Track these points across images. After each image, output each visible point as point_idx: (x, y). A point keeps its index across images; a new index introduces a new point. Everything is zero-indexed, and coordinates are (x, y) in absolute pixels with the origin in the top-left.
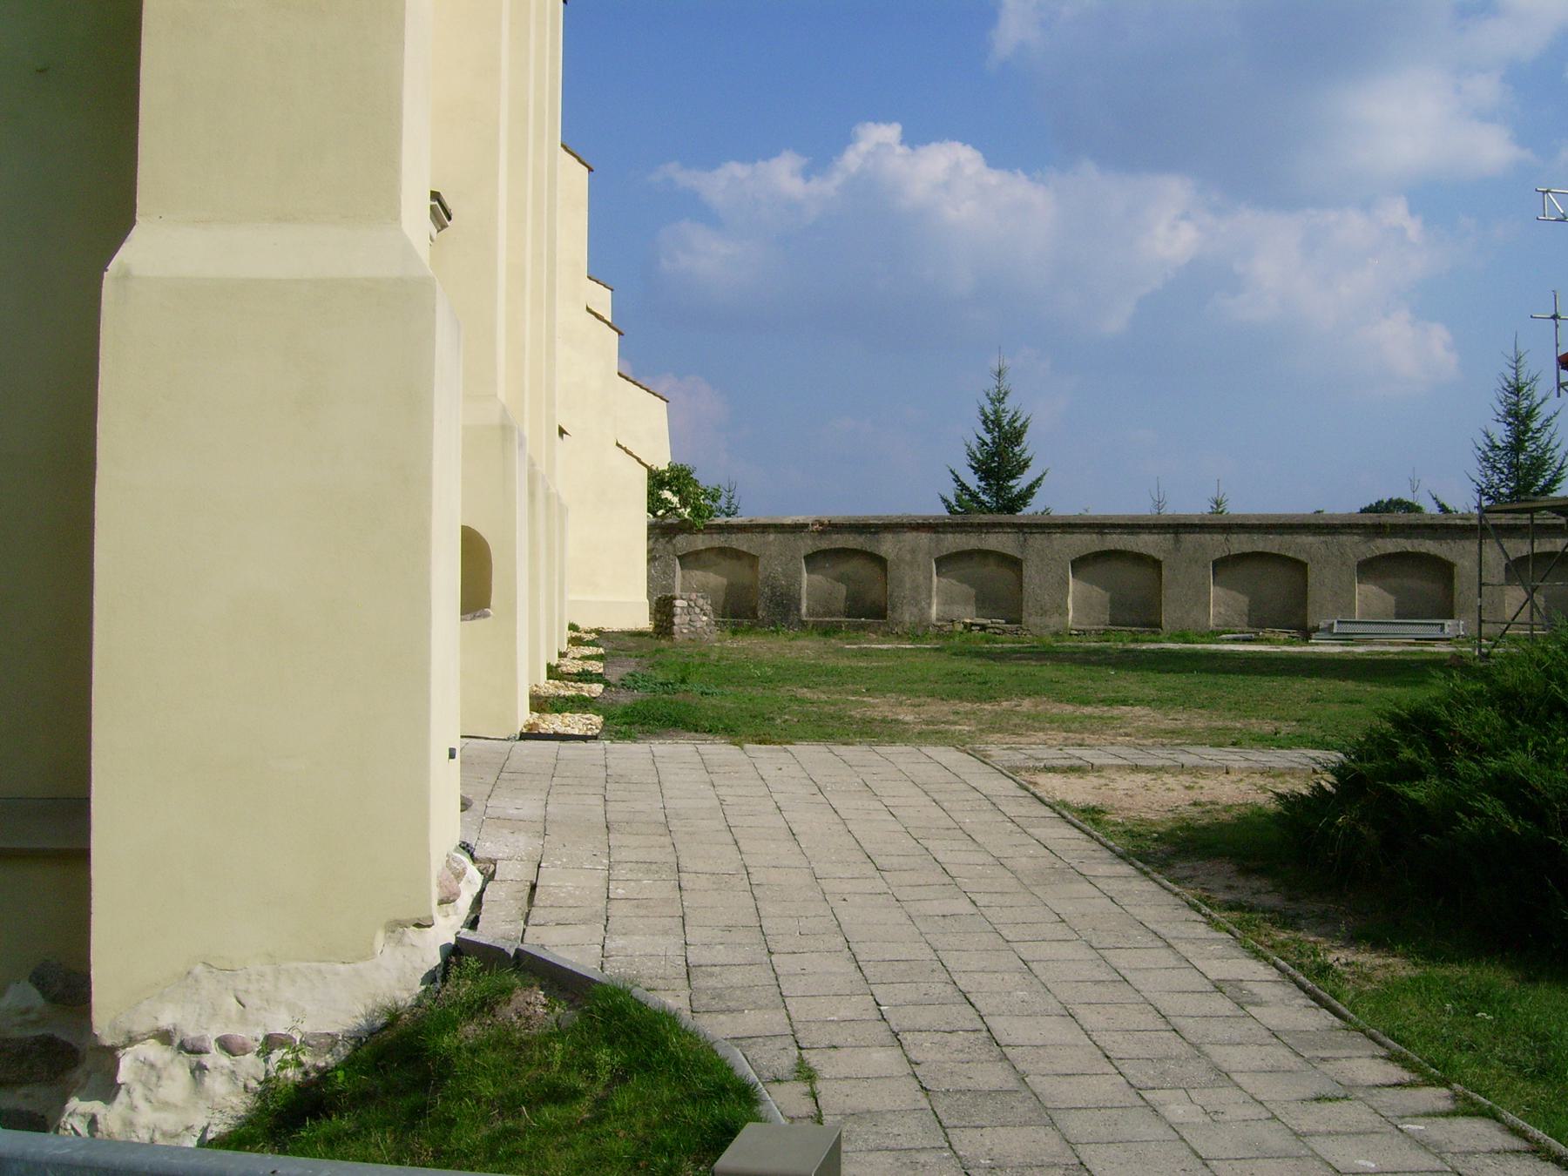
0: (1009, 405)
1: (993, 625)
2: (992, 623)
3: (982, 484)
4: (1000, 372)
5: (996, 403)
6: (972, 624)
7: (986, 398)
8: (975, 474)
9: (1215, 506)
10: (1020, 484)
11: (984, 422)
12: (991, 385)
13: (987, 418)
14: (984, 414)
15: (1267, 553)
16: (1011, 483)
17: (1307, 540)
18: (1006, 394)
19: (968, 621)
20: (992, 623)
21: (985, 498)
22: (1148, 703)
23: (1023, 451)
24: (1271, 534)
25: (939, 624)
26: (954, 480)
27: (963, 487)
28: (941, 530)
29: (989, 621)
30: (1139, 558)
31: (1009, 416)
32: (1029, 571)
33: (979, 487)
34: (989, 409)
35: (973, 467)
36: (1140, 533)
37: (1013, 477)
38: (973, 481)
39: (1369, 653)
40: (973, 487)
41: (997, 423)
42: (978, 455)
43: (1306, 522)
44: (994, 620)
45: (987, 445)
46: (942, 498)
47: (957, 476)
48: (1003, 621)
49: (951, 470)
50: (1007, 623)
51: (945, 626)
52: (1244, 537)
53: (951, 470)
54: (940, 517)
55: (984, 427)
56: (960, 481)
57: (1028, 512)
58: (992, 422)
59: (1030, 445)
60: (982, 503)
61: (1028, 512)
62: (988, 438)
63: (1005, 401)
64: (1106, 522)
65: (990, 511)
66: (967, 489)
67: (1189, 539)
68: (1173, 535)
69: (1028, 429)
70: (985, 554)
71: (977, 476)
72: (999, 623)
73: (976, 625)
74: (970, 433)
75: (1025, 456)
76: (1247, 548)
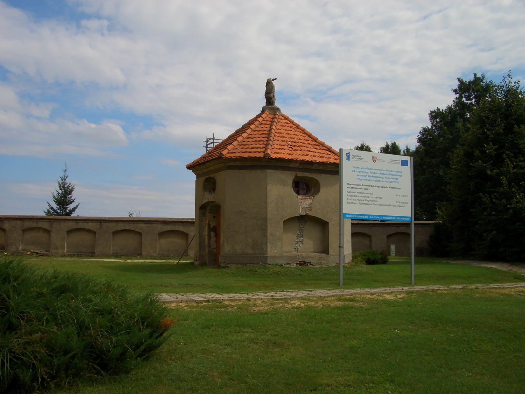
0: (68, 181)
1: (40, 252)
2: (40, 252)
3: (58, 207)
4: (65, 170)
5: (64, 180)
6: (34, 252)
7: (61, 179)
8: (56, 203)
9: (130, 215)
10: (71, 207)
11: (60, 187)
12: (62, 174)
13: (60, 185)
14: (59, 184)
15: (129, 230)
16: (68, 206)
17: (142, 225)
18: (67, 177)
19: (32, 251)
20: (40, 252)
21: (59, 211)
22: (281, 291)
23: (71, 197)
24: (131, 223)
25: (22, 252)
26: (48, 205)
27: (52, 208)
28: (24, 220)
29: (39, 251)
30: (89, 231)
31: (67, 185)
32: (53, 235)
33: (57, 207)
34: (61, 182)
35: (55, 201)
36: (89, 222)
37: (69, 204)
38: (55, 206)
39: (166, 262)
40: (55, 208)
41: (64, 187)
42: (56, 197)
43: (142, 220)
44: (41, 251)
45: (60, 194)
46: (44, 212)
47: (49, 204)
48: (44, 251)
49: (48, 202)
50: (45, 252)
51: (24, 252)
52: (122, 224)
53: (48, 202)
54: (43, 216)
55: (60, 188)
56: (50, 206)
57: (74, 215)
58: (62, 186)
59: (74, 195)
60: (57, 212)
61: (74, 215)
62: (60, 192)
63: (66, 180)
64: (151, 220)
65: (60, 215)
66: (53, 208)
67: (105, 225)
68: (99, 223)
69: (74, 190)
70: (39, 229)
71: (56, 204)
72: (42, 252)
73: (35, 252)
74: (55, 190)
75: (73, 198)
76: (123, 228)
